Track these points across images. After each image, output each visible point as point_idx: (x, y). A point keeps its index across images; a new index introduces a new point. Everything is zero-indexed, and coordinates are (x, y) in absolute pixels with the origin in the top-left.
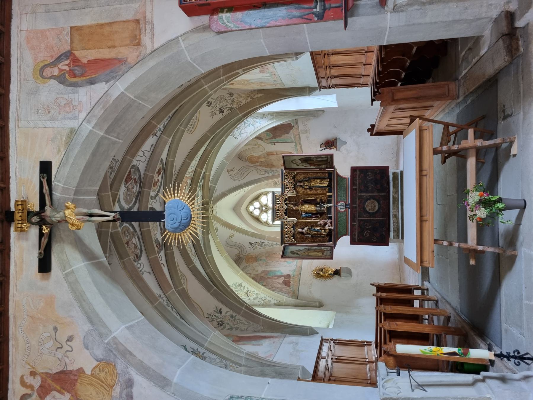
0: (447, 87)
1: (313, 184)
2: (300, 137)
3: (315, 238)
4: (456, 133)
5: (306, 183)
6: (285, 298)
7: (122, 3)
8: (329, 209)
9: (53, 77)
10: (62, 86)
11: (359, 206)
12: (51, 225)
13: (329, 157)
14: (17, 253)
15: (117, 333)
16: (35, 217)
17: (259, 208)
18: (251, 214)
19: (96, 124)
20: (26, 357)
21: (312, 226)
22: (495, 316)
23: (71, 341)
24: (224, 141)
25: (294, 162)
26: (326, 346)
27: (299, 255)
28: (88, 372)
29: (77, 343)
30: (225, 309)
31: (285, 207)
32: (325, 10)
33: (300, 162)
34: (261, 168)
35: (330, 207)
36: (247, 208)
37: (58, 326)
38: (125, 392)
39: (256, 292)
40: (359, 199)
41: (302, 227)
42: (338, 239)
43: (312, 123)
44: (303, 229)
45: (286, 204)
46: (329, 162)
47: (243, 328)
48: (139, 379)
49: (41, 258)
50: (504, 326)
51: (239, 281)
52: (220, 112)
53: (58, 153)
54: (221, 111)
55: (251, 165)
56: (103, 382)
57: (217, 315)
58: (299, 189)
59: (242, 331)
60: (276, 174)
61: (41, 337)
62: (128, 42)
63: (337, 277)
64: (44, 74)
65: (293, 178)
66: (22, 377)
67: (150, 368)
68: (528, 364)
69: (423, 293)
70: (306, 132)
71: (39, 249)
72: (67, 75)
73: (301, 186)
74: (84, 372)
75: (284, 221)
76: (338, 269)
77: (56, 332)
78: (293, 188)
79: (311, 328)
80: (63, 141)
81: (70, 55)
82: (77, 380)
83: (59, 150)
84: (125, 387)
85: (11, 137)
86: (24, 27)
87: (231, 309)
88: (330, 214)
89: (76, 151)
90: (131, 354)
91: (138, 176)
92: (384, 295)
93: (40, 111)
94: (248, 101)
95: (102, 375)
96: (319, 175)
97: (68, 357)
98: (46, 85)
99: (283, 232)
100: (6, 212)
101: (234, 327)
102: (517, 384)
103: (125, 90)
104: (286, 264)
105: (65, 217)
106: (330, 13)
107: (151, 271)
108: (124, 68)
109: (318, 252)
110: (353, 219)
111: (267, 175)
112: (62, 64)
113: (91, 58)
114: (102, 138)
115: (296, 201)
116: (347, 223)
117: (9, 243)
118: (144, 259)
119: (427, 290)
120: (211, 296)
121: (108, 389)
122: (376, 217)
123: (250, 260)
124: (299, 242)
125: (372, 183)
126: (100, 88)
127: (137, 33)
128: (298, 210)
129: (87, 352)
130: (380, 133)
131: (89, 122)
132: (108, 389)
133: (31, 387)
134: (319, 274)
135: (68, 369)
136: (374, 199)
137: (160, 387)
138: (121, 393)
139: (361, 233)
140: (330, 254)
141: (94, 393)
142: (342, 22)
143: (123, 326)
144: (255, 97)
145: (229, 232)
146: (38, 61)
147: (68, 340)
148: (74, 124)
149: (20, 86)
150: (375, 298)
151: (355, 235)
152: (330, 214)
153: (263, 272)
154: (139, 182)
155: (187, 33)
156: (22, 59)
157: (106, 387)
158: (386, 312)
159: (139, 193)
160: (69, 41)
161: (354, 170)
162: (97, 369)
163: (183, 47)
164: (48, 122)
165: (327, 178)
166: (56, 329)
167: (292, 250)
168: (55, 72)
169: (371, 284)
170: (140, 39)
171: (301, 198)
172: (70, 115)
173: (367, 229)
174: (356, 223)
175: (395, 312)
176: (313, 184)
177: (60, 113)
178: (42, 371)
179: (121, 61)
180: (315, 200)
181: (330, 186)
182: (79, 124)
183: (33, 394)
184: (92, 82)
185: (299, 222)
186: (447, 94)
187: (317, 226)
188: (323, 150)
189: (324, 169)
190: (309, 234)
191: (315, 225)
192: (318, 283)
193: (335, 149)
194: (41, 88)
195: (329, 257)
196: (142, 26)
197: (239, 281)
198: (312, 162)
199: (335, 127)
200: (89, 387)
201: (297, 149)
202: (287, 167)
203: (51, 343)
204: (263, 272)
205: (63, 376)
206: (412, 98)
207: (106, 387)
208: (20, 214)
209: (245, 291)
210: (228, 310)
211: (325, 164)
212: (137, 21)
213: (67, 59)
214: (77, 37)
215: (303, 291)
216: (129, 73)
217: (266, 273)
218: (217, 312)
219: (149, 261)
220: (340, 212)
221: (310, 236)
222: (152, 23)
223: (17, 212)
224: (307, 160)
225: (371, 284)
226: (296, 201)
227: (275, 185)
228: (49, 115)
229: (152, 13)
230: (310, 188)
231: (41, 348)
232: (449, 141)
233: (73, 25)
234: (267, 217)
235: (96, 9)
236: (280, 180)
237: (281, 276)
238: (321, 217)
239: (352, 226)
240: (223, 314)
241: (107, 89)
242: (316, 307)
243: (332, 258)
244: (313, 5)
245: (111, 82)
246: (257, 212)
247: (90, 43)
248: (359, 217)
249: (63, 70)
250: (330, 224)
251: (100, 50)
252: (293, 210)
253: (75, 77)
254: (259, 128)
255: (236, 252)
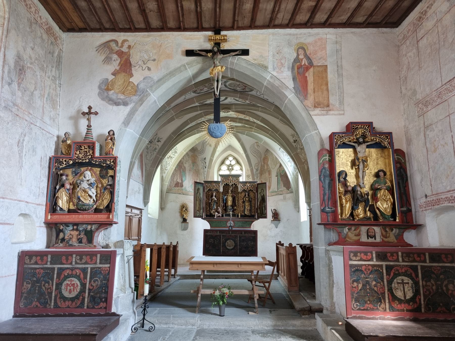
0: (296, 285)
1: (247, 204)
2: (281, 194)
3: (209, 205)
4: (265, 287)
5: (247, 199)
6: (167, 184)
7: (340, 97)
8: (229, 215)
9: (298, 55)
10: (292, 61)
11: (230, 236)
12: (212, 57)
13: (265, 215)
14: (197, 36)
15: (153, 96)
16: (217, 49)
17: (230, 164)
18: (226, 158)
19: (270, 81)
20: (139, 43)
21: (217, 203)
22: (162, 305)
23: (148, 70)
24: (276, 143)
25: (262, 190)
26: (137, 212)
27: (197, 194)
28: (131, 80)
29: (146, 73)
30: (160, 144)
31: (231, 184)
32: (327, 213)
33: (262, 195)
34: (260, 166)
35: (230, 216)
36: (230, 155)
37: (156, 61)
38: (121, 101)
39: (171, 163)
40: (235, 235)
41: (216, 196)
42: (208, 221)
43: (290, 204)
44: (215, 197)
45: (232, 185)
46: (261, 216)
47: (147, 156)
48: (127, 109)
49: (194, 51)
50: (158, 309)
51: (179, 152)
52: (294, 140)
53: (254, 59)
54: (295, 141)
55: (262, 159)
56: (126, 88)
57: (157, 139)
58: (243, 194)
59: (146, 156)
60: (255, 177)
61: (150, 52)
62: (316, 101)
63: (182, 220)
64: (300, 50)
65: (251, 189)
66: (128, 41)
67: (134, 115)
68: (142, 312)
69: (172, 275)
70: (285, 199)
71: (199, 50)
72: (299, 64)
73: (245, 195)
74: (131, 77)
75: (221, 183)
76: (187, 221)
77: (152, 60)
78: (244, 189)
79: (148, 202)
80: (261, 62)
81: (311, 65)
82: (126, 73)
83: (255, 60)
84: (123, 101)
85: (264, 30)
86: (328, 36)
87: (160, 149)
88: (225, 216)
89: (255, 70)
90: (141, 104)
91: (248, 90)
92: (171, 249)
93: (278, 48)
94: (302, 159)
95: (129, 88)
96: (253, 208)
97: (139, 68)
98: (293, 51)
99: (213, 183)
100: (220, 29)
101: (149, 150)
102: (132, 307)
103: (289, 99)
104: (191, 184)
105: (217, 67)
106: (325, 215)
107: (185, 100)
108: (302, 98)
109: (199, 207)
110: (221, 231)
111: (254, 170)
112: (306, 60)
113: (308, 79)
114: (263, 85)
115: (235, 192)
116: (219, 227)
117: (202, 31)
118: (193, 95)
119: (175, 278)
120: (169, 135)
121: (122, 91)
122: (222, 247)
123: (193, 158)
124: (206, 193)
125: (246, 245)
126: (290, 84)
127: (322, 106)
128: (228, 194)
129: (142, 79)
130: (278, 249)
131: (271, 77)
132: (122, 91)
133: (122, 46)
134: (184, 207)
135: (132, 68)
136: (235, 247)
137: (124, 121)
138: (120, 99)
139: (212, 237)
140: (197, 216)
141: (120, 83)
142: (320, 222)
143: (156, 99)
144: (305, 165)
145: (213, 145)
146: (308, 45)
147: (148, 68)
148: (270, 69)
149: (294, 35)
150: (169, 244)
151: (210, 233)
152: (225, 216)
153: (184, 168)
154: (244, 91)
155: (320, 135)
156: (309, 36)
157: (123, 90)
158: (162, 249)
159: (237, 91)
160: (319, 65)
161: (255, 232)
162: (133, 85)
163: (312, 133)
164: (271, 53)
165: (251, 214)
166: (154, 60)
167: (200, 189)
168: (301, 57)
169: (177, 242)
170: (318, 107)
171: (237, 196)
172: (275, 66)
173: (214, 241)
174: (218, 234)
175: (162, 254)
176: (247, 204)
177: (277, 60)
178: (131, 52)
179: (306, 97)
180: (235, 206)
181: (245, 216)
182: (270, 72)
183: (118, 47)
184: (294, 79)
185: (220, 194)
186: (292, 285)
187: (217, 207)
188: (272, 211)
189: (257, 212)
190: (211, 201)
191: (218, 205)
192: (177, 207)
193: (272, 220)
194: (292, 48)
195: (195, 215)
196: (326, 109)
197: (179, 152)
198: (262, 204)
199: (288, 220)
200: (123, 80)
201: (272, 192)
202: (259, 186)
203: (147, 58)
204: (185, 168)
205: (129, 64)
206: (290, 266)
207: (123, 90)
208: (219, 38)
209: (172, 155)
210: (160, 146)
211: (260, 212)
212: (328, 106)
213: (308, 64)
214: (321, 69)
215: (172, 196)
216: (299, 101)
217: (184, 170)
218: (158, 139)
219: (193, 98)
220: (227, 223)
221: (210, 202)
222: (327, 114)
223: (220, 37)
224: (264, 200)
225: (177, 242)
226: (235, 192)
227: (248, 176)
228: (276, 54)
229: (332, 114)
230: (244, 202)
231: (144, 51)
232: (259, 282)
233: (328, 67)
234: (224, 171)
235: (337, 81)
236: (251, 180)
237: (182, 180)
238: (223, 209)
239: (217, 231)
240: (157, 143)
241: (290, 88)
242: (161, 205)
243: (195, 216)
244: (330, 207)
245: (294, 91)
246: (227, 162)
247: (317, 78)
248: (223, 235)
249: (302, 61)
250: (218, 215)
251: (313, 84)
252: (228, 189)
253: (298, 69)
254: (287, 165)
255: (199, 149)
